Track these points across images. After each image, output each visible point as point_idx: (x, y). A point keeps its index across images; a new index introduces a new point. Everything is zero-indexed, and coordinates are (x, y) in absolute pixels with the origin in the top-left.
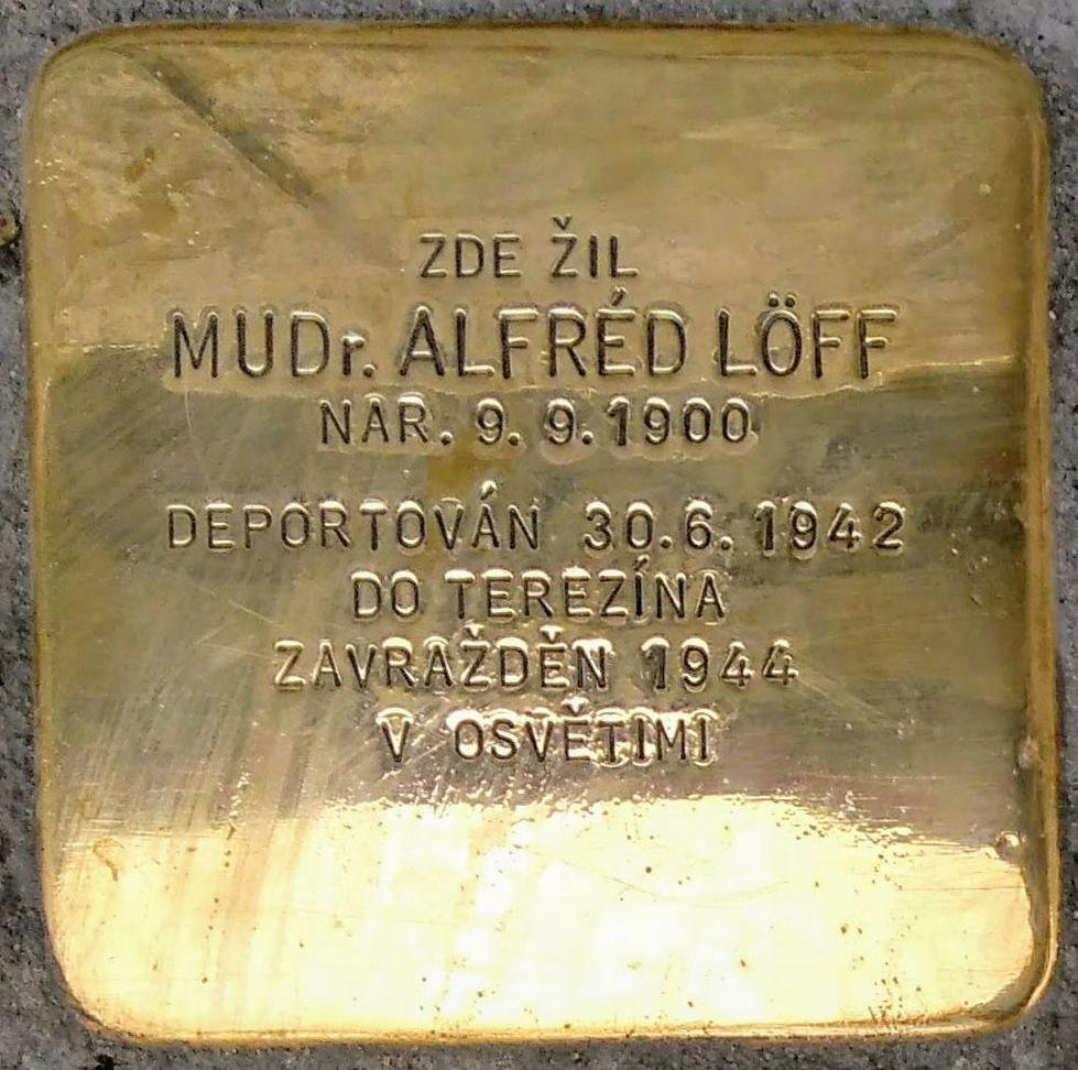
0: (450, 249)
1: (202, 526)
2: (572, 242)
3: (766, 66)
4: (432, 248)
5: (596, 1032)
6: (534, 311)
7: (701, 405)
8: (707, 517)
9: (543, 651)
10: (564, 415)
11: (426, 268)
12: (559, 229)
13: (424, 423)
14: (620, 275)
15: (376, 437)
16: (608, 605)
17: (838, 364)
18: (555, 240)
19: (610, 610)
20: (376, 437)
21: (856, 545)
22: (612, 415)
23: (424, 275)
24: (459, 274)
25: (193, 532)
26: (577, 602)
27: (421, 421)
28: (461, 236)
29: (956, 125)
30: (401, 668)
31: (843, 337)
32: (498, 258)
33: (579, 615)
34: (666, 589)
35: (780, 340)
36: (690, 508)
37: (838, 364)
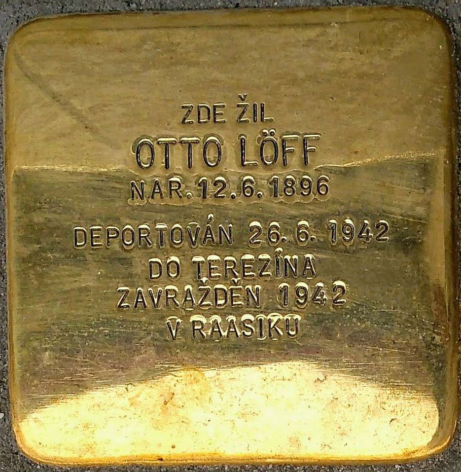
0: (194, 112)
1: (88, 235)
2: (245, 106)
3: (121, 34)
4: (186, 111)
5: (387, 457)
6: (197, 139)
7: (251, 180)
8: (307, 228)
9: (232, 289)
10: (307, 183)
11: (185, 119)
12: (241, 101)
13: (180, 189)
14: (217, 122)
15: (157, 196)
16: (262, 272)
17: (294, 161)
18: (238, 106)
19: (263, 274)
20: (157, 196)
21: (370, 239)
22: (199, 185)
23: (183, 122)
24: (199, 122)
25: (85, 239)
26: (248, 270)
27: (178, 189)
28: (200, 105)
29: (421, 49)
30: (173, 298)
31: (297, 149)
32: (215, 114)
33: (250, 276)
34: (289, 264)
35: (269, 152)
36: (300, 223)
37: (294, 161)
